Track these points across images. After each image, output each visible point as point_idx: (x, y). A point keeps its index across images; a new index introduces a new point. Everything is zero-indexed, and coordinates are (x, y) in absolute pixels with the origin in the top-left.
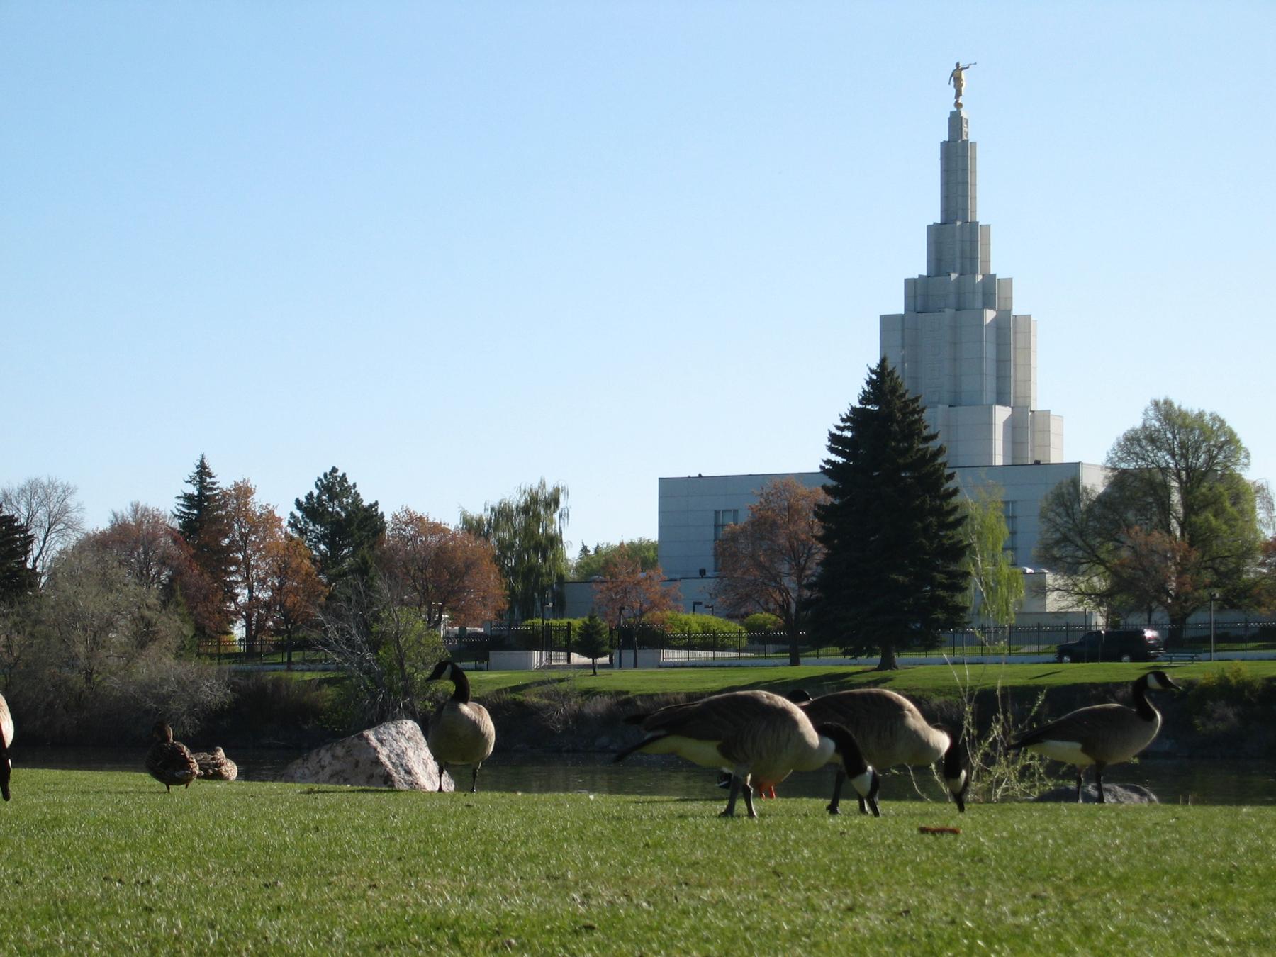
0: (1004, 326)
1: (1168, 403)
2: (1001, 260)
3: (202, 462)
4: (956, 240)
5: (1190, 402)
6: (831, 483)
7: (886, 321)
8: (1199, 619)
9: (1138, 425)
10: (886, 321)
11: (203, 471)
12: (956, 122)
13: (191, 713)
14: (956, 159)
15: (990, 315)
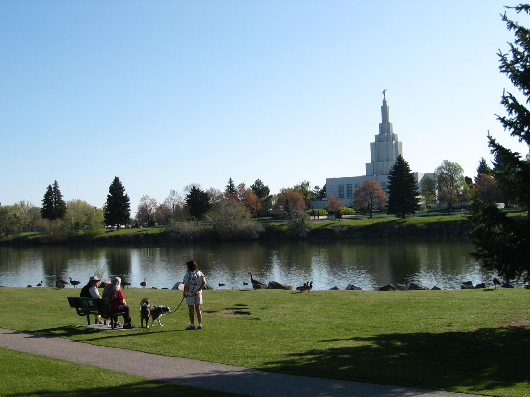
0: (397, 143)
1: (447, 161)
2: (395, 130)
3: (231, 179)
4: (385, 126)
5: (451, 160)
6: (390, 181)
7: (372, 144)
8: (456, 205)
9: (440, 165)
10: (372, 144)
11: (231, 181)
12: (384, 102)
13: (257, 233)
14: (385, 109)
15: (394, 142)
